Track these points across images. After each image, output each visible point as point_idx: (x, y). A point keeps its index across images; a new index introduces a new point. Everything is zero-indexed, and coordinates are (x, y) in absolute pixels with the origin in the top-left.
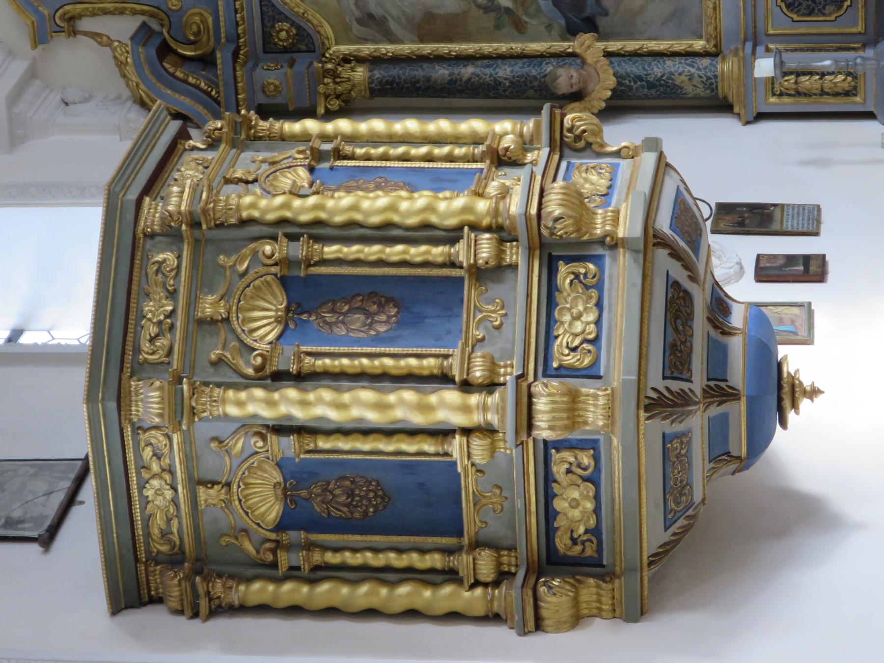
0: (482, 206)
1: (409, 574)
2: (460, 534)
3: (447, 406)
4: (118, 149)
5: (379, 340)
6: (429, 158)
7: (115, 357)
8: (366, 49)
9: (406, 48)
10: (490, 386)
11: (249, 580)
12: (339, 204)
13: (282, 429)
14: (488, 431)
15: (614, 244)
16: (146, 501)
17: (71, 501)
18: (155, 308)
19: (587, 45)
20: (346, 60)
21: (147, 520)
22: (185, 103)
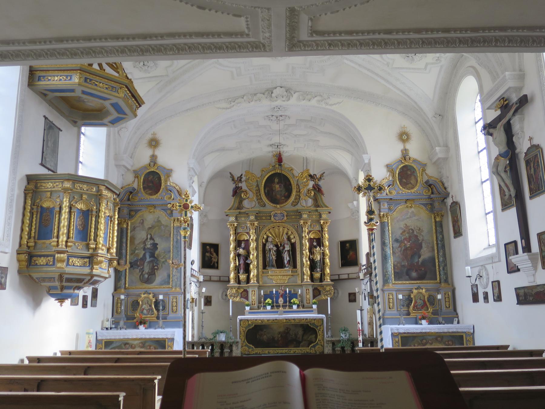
0: (100, 246)
1: (30, 230)
2: (38, 239)
3: (63, 238)
4: (114, 182)
5: (76, 227)
6: (110, 237)
7: (76, 179)
8: (129, 228)
9: (129, 234)
10: (66, 246)
11: (31, 200)
12: (102, 220)
13: (61, 208)
14: (58, 245)
15: (92, 269)
16: (48, 183)
17: (49, 169)
18: (85, 187)
19: (128, 267)
20: (127, 224)
21: (45, 183)
22: (121, 196)
